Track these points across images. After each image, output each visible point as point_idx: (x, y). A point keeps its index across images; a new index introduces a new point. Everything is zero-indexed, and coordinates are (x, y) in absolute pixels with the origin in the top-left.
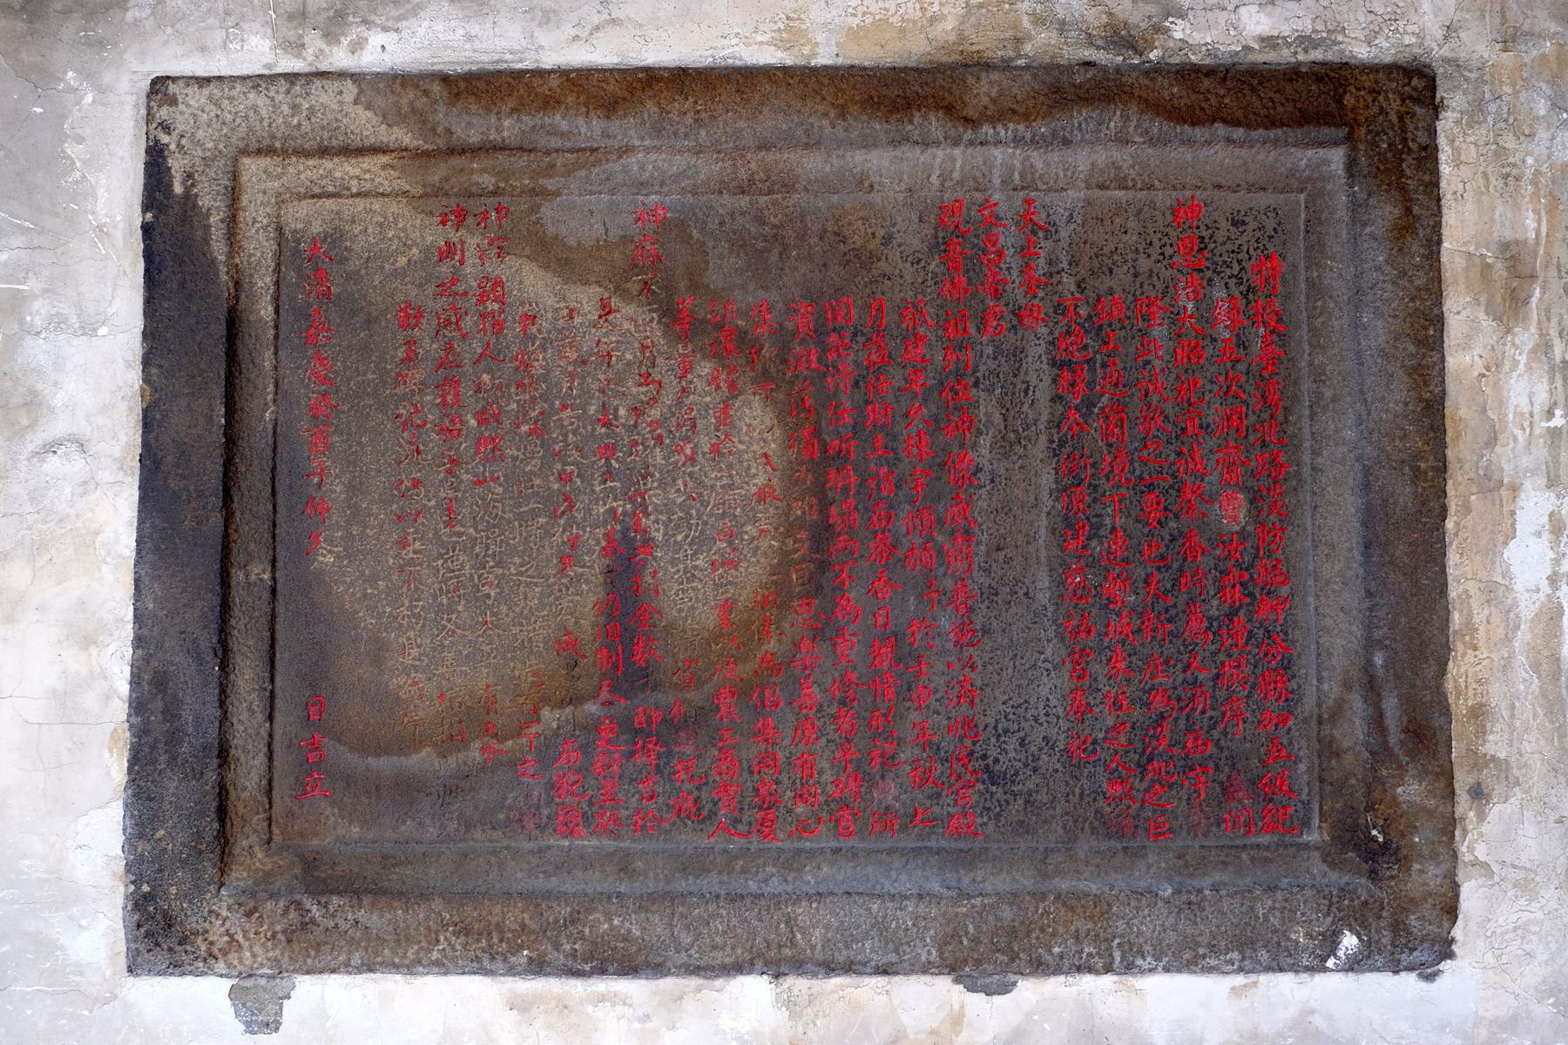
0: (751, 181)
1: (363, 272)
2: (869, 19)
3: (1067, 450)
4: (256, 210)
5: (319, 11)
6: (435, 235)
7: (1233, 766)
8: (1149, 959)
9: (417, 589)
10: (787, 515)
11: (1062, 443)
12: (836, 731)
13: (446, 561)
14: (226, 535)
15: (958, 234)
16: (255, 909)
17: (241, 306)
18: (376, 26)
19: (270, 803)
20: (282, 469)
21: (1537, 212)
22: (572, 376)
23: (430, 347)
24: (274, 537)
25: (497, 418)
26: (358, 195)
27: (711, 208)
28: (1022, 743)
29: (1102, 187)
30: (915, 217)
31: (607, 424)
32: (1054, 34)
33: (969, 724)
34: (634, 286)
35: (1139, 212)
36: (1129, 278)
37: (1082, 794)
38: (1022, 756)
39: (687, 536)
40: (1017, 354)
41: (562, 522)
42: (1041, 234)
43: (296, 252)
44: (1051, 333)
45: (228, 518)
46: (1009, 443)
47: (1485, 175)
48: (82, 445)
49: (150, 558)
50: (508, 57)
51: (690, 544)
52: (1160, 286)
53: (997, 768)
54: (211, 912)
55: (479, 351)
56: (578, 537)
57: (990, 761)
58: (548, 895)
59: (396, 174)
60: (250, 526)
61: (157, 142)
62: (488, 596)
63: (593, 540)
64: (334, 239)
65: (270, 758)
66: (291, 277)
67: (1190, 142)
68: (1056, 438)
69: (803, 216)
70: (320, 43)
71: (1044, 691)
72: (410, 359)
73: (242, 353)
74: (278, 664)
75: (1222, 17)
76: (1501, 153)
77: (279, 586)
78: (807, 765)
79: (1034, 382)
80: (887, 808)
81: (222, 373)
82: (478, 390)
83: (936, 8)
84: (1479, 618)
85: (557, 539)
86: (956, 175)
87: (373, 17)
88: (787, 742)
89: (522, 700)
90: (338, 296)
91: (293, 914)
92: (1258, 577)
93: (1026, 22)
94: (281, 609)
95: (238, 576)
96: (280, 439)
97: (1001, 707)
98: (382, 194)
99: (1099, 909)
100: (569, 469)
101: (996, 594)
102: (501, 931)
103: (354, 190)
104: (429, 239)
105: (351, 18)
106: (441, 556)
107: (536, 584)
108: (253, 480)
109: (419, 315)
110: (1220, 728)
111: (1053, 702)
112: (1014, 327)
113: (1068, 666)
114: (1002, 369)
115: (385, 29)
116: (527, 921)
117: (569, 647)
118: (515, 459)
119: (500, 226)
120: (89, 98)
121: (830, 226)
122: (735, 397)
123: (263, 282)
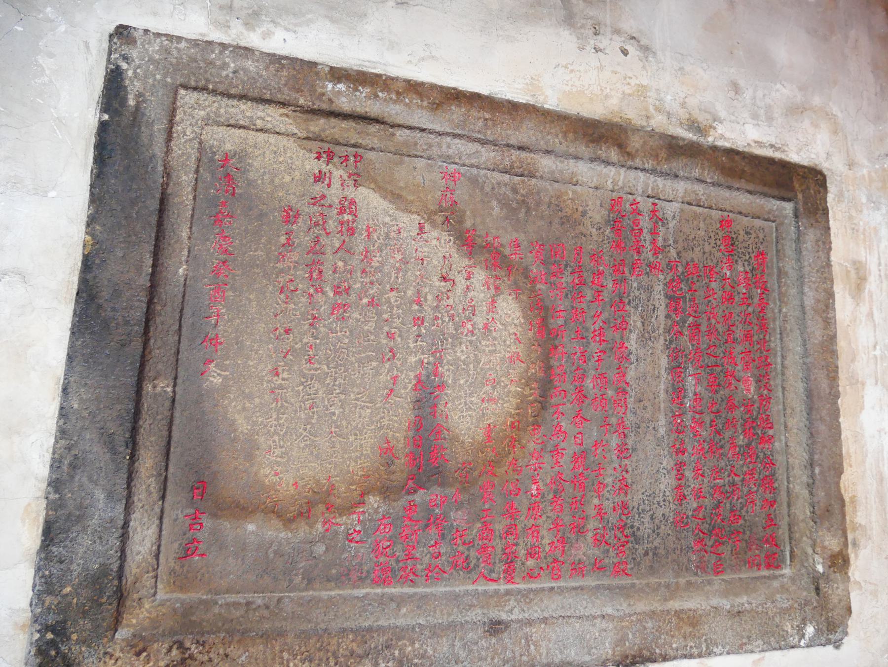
0: (512, 167)
1: (260, 182)
2: (575, 89)
3: (673, 346)
4: (185, 129)
5: (242, 8)
6: (313, 165)
7: (751, 531)
8: (720, 647)
9: (282, 406)
10: (527, 371)
11: (671, 342)
12: (552, 510)
13: (305, 387)
14: (143, 356)
15: (621, 217)
16: (144, 650)
17: (169, 191)
18: (281, 26)
19: (158, 564)
20: (188, 311)
21: (865, 248)
22: (399, 270)
23: (304, 239)
24: (177, 360)
25: (347, 290)
26: (261, 130)
27: (487, 178)
28: (652, 518)
29: (689, 204)
30: (598, 203)
31: (419, 303)
32: (665, 118)
33: (624, 506)
34: (439, 219)
35: (705, 220)
36: (701, 255)
37: (681, 549)
38: (651, 526)
39: (467, 381)
40: (649, 289)
41: (387, 366)
42: (660, 223)
43: (212, 160)
44: (665, 279)
45: (146, 343)
46: (645, 338)
47: (845, 227)
48: (24, 277)
49: (78, 369)
50: (366, 64)
51: (469, 386)
52: (715, 261)
53: (639, 533)
54: (105, 653)
55: (337, 245)
56: (397, 377)
57: (635, 529)
58: (370, 630)
59: (291, 121)
60: (160, 352)
61: (118, 67)
62: (334, 414)
63: (408, 379)
64: (242, 155)
65: (161, 530)
66: (206, 176)
67: (730, 188)
68: (668, 338)
69: (538, 193)
70: (241, 28)
71: (662, 487)
72: (289, 243)
73: (167, 225)
74: (172, 456)
75: (738, 127)
76: (851, 218)
77: (177, 397)
78: (535, 530)
79: (657, 306)
80: (579, 560)
81: (153, 235)
82: (335, 271)
83: (608, 91)
84: (852, 450)
85: (382, 378)
86: (620, 183)
87: (279, 20)
88: (523, 518)
89: (354, 487)
90: (240, 195)
91: (174, 652)
92: (759, 425)
93: (651, 108)
94: (177, 414)
95: (148, 387)
96: (188, 290)
97: (641, 496)
98: (278, 133)
99: (693, 620)
100: (393, 331)
101: (639, 427)
102: (336, 657)
103: (259, 127)
104: (308, 167)
105: (263, 17)
106: (302, 384)
107: (368, 407)
108: (165, 317)
109: (297, 216)
110: (745, 509)
111: (667, 493)
112: (647, 273)
113: (675, 472)
114: (642, 296)
115: (287, 29)
116: (355, 648)
117: (387, 452)
118: (358, 320)
119: (356, 167)
120: (62, 28)
121: (553, 200)
122: (498, 295)
123: (186, 178)
